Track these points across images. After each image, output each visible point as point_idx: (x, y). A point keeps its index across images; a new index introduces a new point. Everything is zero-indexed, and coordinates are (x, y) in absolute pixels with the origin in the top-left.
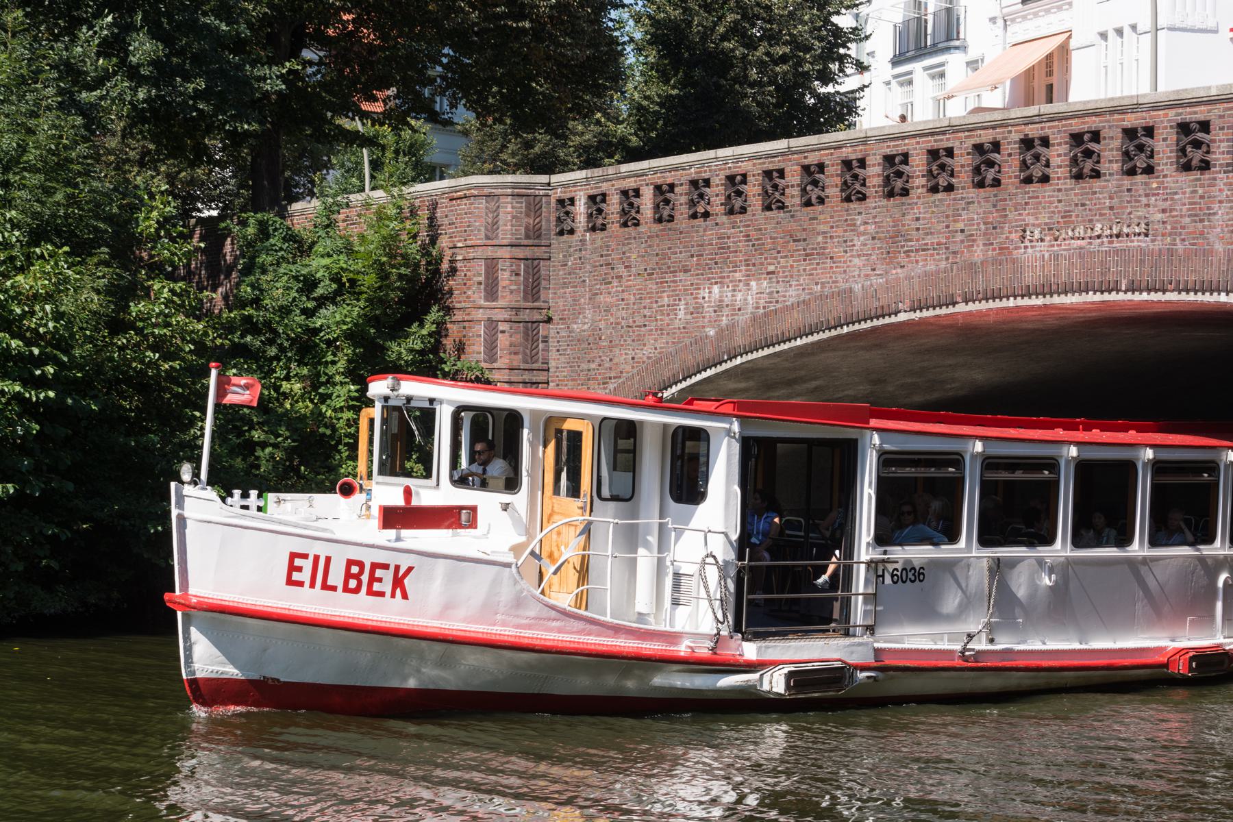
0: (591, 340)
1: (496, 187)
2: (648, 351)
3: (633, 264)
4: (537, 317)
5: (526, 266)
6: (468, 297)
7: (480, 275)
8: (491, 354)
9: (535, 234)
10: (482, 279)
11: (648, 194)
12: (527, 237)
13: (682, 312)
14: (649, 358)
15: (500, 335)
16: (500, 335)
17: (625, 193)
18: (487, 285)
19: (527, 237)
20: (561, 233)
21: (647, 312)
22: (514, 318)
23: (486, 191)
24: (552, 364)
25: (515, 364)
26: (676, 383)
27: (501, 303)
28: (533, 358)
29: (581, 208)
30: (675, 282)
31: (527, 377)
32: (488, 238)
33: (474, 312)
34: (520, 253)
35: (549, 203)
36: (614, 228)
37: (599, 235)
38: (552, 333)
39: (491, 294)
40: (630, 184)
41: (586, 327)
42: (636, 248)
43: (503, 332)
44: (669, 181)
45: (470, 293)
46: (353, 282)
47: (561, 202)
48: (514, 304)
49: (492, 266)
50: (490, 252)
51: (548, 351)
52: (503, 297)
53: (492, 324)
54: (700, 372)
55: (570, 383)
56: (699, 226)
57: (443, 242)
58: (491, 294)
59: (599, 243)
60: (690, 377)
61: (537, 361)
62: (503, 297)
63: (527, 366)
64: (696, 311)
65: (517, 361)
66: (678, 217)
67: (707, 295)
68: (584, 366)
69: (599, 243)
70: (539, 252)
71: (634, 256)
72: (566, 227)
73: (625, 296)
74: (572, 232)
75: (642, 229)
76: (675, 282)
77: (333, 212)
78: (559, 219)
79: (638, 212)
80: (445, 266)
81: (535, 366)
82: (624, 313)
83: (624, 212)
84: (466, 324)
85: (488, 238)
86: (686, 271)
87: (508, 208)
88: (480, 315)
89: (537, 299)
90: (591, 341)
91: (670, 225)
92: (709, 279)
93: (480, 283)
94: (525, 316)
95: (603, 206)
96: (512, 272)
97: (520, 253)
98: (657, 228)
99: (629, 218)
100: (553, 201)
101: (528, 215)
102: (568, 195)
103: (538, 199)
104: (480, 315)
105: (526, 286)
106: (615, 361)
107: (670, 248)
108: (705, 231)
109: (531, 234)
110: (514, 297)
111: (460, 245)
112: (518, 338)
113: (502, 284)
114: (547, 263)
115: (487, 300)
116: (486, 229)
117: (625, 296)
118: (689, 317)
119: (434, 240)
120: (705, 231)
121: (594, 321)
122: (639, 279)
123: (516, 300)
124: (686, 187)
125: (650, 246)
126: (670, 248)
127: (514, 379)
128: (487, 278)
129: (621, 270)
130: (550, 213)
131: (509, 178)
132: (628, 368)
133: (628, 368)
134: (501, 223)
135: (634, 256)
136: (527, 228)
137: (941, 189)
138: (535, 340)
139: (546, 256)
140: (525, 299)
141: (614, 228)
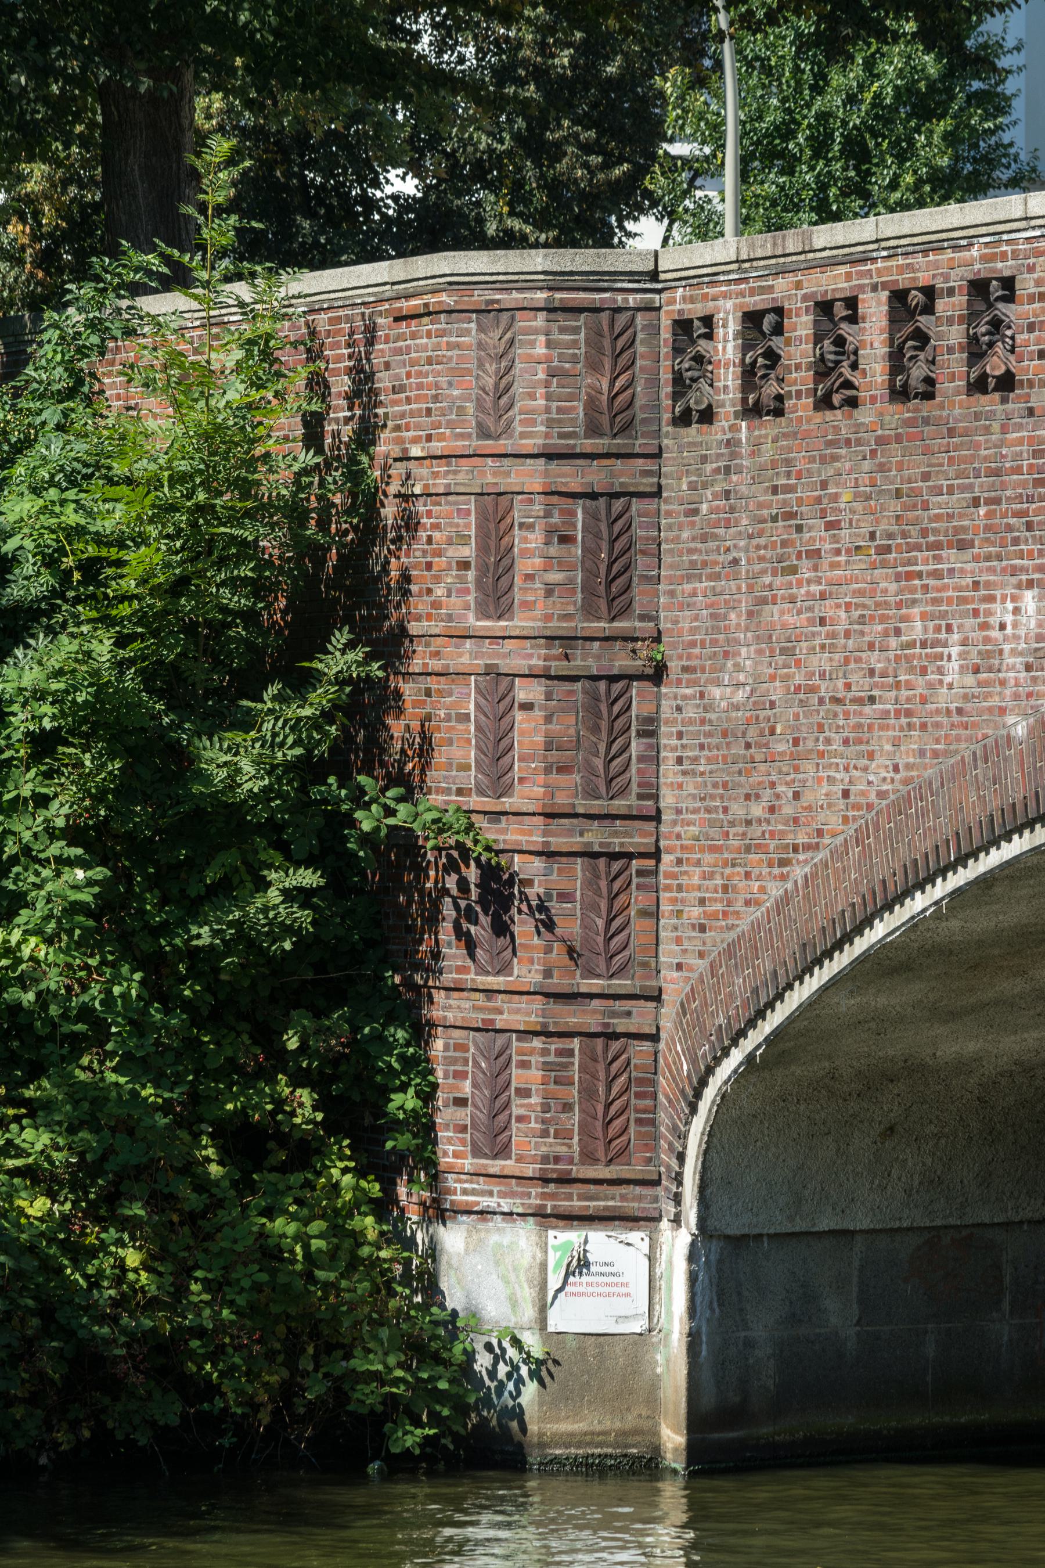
0: (752, 733)
1: (505, 287)
2: (877, 779)
3: (845, 516)
4: (621, 661)
5: (592, 516)
6: (436, 605)
7: (464, 540)
8: (497, 776)
9: (615, 420)
10: (468, 552)
11: (875, 309)
12: (593, 430)
13: (955, 665)
14: (882, 795)
15: (519, 716)
16: (519, 716)
17: (824, 307)
18: (483, 570)
19: (593, 430)
20: (683, 419)
21: (875, 660)
22: (558, 667)
23: (479, 297)
24: (668, 799)
25: (562, 800)
26: (943, 872)
27: (520, 623)
28: (613, 782)
29: (727, 348)
30: (937, 574)
31: (594, 837)
32: (484, 433)
33: (450, 648)
34: (572, 477)
35: (654, 330)
36: (801, 408)
37: (769, 427)
38: (667, 710)
39: (496, 597)
40: (835, 282)
41: (740, 695)
42: (846, 464)
43: (527, 707)
44: (924, 278)
45: (439, 591)
46: (91, 568)
47: (683, 326)
48: (556, 626)
49: (495, 511)
50: (491, 475)
51: (657, 760)
52: (527, 605)
53: (497, 682)
54: (995, 842)
55: (708, 858)
56: (990, 416)
57: (385, 446)
58: (496, 597)
59: (768, 451)
60: (974, 854)
61: (624, 791)
62: (527, 605)
63: (597, 806)
64: (984, 664)
65: (568, 792)
66: (944, 387)
67: (1009, 619)
68: (738, 810)
69: (768, 451)
70: (627, 475)
71: (846, 497)
72: (995, 366)
73: (827, 609)
74: (707, 416)
75: (865, 415)
76: (937, 574)
77: (82, 352)
78: (678, 379)
79: (854, 366)
80: (389, 511)
81: (619, 805)
82: (821, 661)
83: (823, 370)
84: (432, 683)
85: (484, 433)
86: (962, 546)
87: (536, 345)
88: (465, 656)
89: (625, 611)
90: (747, 740)
91: (926, 408)
92: (1014, 571)
93: (464, 565)
94: (588, 660)
95: (776, 342)
96: (549, 532)
97: (572, 477)
98: (897, 414)
99: (834, 389)
100: (666, 322)
101: (594, 366)
102: (698, 310)
103: (622, 319)
104: (465, 656)
105: (590, 574)
106: (807, 798)
107: (926, 477)
108: (1004, 429)
109: (605, 420)
110: (558, 605)
111: (416, 451)
112: (566, 726)
113: (525, 565)
114: (651, 505)
115: (483, 613)
116: (480, 406)
117: (827, 609)
118: (970, 680)
119: (366, 435)
120: (1004, 429)
121: (758, 680)
122: (860, 562)
123: (565, 614)
124: (960, 300)
125: (882, 468)
126: (926, 477)
127: (559, 842)
128: (483, 548)
129: (816, 535)
130: (656, 359)
131: (538, 260)
132: (834, 821)
133: (834, 821)
134: (518, 389)
135: (846, 497)
136: (591, 405)
137: (992, 383)
138: (617, 732)
139: (647, 484)
140: (589, 611)
141: (801, 408)
